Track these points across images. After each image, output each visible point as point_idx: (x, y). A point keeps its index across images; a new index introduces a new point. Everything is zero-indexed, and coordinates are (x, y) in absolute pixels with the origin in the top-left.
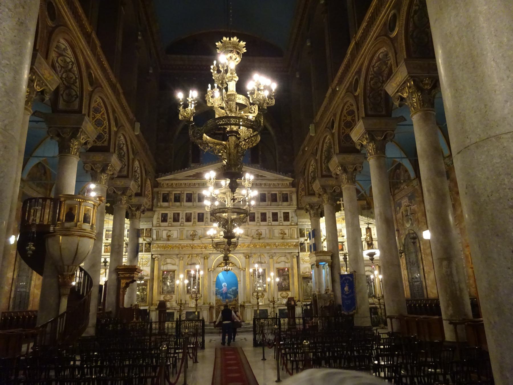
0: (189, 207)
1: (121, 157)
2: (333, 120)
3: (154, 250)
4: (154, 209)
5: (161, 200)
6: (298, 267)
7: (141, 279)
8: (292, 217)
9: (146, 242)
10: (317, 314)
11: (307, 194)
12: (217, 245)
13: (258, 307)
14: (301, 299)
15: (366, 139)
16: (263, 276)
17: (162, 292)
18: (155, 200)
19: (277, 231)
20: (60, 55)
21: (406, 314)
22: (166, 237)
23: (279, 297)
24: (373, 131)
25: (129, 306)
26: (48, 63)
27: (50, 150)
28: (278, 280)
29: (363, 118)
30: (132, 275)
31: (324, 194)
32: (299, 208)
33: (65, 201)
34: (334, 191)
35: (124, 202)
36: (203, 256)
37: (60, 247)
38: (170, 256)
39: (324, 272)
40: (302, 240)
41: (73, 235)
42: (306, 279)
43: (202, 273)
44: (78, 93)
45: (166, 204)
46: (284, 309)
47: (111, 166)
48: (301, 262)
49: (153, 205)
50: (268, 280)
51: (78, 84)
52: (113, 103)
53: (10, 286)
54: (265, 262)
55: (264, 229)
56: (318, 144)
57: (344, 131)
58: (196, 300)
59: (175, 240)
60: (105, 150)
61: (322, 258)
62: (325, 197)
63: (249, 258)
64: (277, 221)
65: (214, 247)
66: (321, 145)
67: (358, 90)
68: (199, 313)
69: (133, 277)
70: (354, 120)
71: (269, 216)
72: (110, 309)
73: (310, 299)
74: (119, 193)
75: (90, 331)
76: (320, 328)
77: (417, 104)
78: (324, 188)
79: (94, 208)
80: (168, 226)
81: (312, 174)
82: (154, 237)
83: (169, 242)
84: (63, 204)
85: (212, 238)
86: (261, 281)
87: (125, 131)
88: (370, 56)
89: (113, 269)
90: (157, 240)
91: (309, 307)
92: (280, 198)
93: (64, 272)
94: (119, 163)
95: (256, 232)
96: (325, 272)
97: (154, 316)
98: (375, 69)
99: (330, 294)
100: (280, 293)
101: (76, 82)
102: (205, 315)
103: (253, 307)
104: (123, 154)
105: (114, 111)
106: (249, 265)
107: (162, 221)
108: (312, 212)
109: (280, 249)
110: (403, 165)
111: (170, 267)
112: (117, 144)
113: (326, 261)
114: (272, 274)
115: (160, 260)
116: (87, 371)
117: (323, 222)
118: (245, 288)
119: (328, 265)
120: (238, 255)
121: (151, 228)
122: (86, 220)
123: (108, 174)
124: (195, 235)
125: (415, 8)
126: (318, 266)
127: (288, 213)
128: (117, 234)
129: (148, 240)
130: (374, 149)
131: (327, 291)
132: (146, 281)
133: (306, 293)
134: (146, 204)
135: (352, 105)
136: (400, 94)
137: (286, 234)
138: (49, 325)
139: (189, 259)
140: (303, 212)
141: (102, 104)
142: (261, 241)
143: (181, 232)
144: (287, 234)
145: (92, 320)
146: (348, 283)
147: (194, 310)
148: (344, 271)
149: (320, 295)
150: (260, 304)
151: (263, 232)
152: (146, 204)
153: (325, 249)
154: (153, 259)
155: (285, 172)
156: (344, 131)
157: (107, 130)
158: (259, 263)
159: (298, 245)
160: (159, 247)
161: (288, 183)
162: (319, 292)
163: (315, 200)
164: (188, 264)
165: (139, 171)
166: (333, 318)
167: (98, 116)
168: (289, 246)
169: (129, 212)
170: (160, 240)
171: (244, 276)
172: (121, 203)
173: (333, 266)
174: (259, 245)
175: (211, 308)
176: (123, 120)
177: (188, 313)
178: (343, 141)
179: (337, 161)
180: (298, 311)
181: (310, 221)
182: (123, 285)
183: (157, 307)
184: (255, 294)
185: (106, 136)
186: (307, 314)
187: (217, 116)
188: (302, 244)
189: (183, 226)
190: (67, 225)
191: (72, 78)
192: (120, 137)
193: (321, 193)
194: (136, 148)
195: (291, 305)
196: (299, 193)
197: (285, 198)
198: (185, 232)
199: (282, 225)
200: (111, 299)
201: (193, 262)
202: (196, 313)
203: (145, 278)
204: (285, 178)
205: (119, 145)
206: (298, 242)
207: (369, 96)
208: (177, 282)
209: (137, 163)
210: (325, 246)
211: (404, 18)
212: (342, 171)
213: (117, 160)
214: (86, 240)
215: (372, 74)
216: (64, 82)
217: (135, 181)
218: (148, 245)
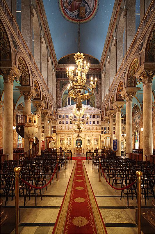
0: (67, 119)
20: (21, 64)
26: (16, 67)
27: (22, 100)
32: (102, 120)
35: (47, 117)
42: (103, 142)
48: (101, 137)
59: (63, 129)
70: (122, 89)
74: (45, 114)
75: (40, 154)
76: (106, 156)
88: (132, 61)
94: (44, 104)
97: (58, 151)
98: (132, 68)
102: (72, 151)
105: (31, 68)
116: (148, 182)
125: (151, 39)
145: (40, 151)
163: (107, 117)
167: (36, 87)
171: (84, 141)
180: (100, 151)
182: (48, 142)
186: (102, 152)
187: (106, 227)
190: (29, 123)
191: (26, 73)
195: (97, 150)
198: (66, 127)
211: (146, 44)
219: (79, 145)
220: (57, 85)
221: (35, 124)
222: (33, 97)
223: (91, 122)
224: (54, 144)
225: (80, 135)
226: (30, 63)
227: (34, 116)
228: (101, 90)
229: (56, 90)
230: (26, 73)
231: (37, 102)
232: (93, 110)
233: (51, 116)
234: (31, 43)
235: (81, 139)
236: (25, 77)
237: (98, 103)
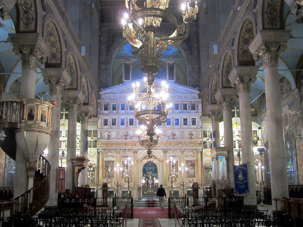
0: (123, 114)
1: (71, 74)
2: (233, 38)
3: (99, 146)
4: (98, 116)
5: (103, 109)
7: (90, 167)
8: (198, 122)
9: (93, 140)
10: (215, 195)
11: (210, 103)
12: (142, 143)
13: (172, 189)
14: (203, 184)
15: (263, 50)
16: (176, 166)
17: (105, 177)
18: (99, 109)
19: (186, 133)
21: (288, 197)
22: (107, 136)
23: (188, 182)
24: (269, 43)
25: (82, 186)
28: (187, 169)
29: (236, 67)
30: (82, 164)
31: (223, 102)
32: (203, 115)
33: (27, 104)
34: (232, 100)
36: (133, 151)
37: (25, 140)
38: (110, 151)
39: (221, 163)
40: (205, 139)
41: (34, 131)
42: (208, 169)
43: (132, 163)
44: (34, 17)
45: (106, 112)
46: (191, 191)
47: (63, 79)
48: (204, 156)
49: (97, 113)
50: (180, 169)
51: (33, 9)
52: (63, 28)
53: (4, 169)
56: (220, 60)
57: (242, 47)
58: (128, 183)
60: (58, 66)
61: (220, 152)
62: (224, 104)
63: (166, 153)
64: (187, 125)
65: (141, 144)
66: (222, 61)
67: (257, 7)
68: (130, 192)
69: (83, 165)
71: (181, 121)
72: (68, 188)
73: (210, 184)
77: (267, 61)
78: (224, 97)
79: (48, 110)
80: (108, 129)
81: (214, 87)
82: (99, 136)
83: (109, 141)
84: (25, 107)
85: (139, 137)
86: (174, 170)
87: (74, 52)
89: (69, 159)
90: (101, 138)
91: (208, 190)
92: (189, 107)
93: (30, 159)
95: (172, 134)
96: (222, 163)
97: (100, 194)
99: (226, 181)
100: (188, 179)
101: (32, 7)
102: (135, 195)
103: (168, 189)
104: (73, 71)
105: (64, 35)
106: (165, 158)
107: (104, 125)
108: (213, 117)
109: (189, 146)
110: (286, 78)
111: (111, 159)
112: (67, 63)
113: (224, 155)
114: (183, 164)
115: (103, 153)
117: (222, 126)
118: (163, 174)
119: (225, 158)
120: (158, 151)
121: (96, 130)
122: (43, 119)
123: (61, 86)
124: (128, 135)
126: (217, 159)
128: (71, 135)
129: (95, 138)
130: (268, 59)
131: (223, 177)
132: (94, 169)
133: (207, 179)
134: (92, 111)
135: (251, 23)
136: (298, 2)
137: (193, 135)
138: (20, 198)
139: (123, 153)
140: (207, 118)
141: (54, 28)
142: (174, 140)
143: (118, 133)
144: (194, 135)
146: (242, 172)
147: (127, 190)
148: (237, 164)
149: (218, 180)
150: (174, 186)
152: (92, 111)
153: (222, 146)
154: (98, 153)
155: (194, 86)
157: (59, 50)
158: (173, 156)
160: (102, 144)
162: (218, 178)
163: (216, 107)
164: (123, 157)
165: (86, 86)
166: (228, 199)
167: (52, 39)
168: (195, 144)
169: (80, 117)
170: (103, 139)
171: (163, 166)
172: (73, 110)
173: (229, 159)
174: (174, 143)
175: (139, 189)
176: (72, 43)
177: (123, 192)
178: (241, 56)
179: (236, 73)
180: (201, 192)
181: (211, 124)
183: (101, 187)
184: (170, 179)
185: (59, 55)
186: (209, 195)
188: (205, 142)
189: (119, 129)
190: (29, 122)
191: (28, 4)
192: (70, 58)
193: (221, 102)
194: (82, 67)
195: (196, 188)
196: (204, 103)
197: (193, 108)
198: (120, 133)
199: (191, 128)
200: (68, 180)
201: (126, 155)
202: (129, 192)
203: (94, 166)
204: (194, 91)
205: (70, 64)
206: (202, 141)
207: (267, 11)
208: (115, 169)
209: (84, 80)
210: (222, 144)
212: (240, 81)
213: (69, 76)
214: (43, 134)
215: (226, 64)
216: (23, 7)
217: (83, 94)
218: (95, 143)
219: (150, 177)
220: (102, 38)
221: (43, 124)
222: (42, 58)
223: (178, 120)
224: (92, 174)
225: (154, 152)
226: (65, 30)
227: (41, 104)
229: (100, 48)
230: (28, 4)
231: (52, 72)
232: (181, 91)
233: (85, 107)
235: (155, 161)
236: (26, 12)
237: (194, 75)
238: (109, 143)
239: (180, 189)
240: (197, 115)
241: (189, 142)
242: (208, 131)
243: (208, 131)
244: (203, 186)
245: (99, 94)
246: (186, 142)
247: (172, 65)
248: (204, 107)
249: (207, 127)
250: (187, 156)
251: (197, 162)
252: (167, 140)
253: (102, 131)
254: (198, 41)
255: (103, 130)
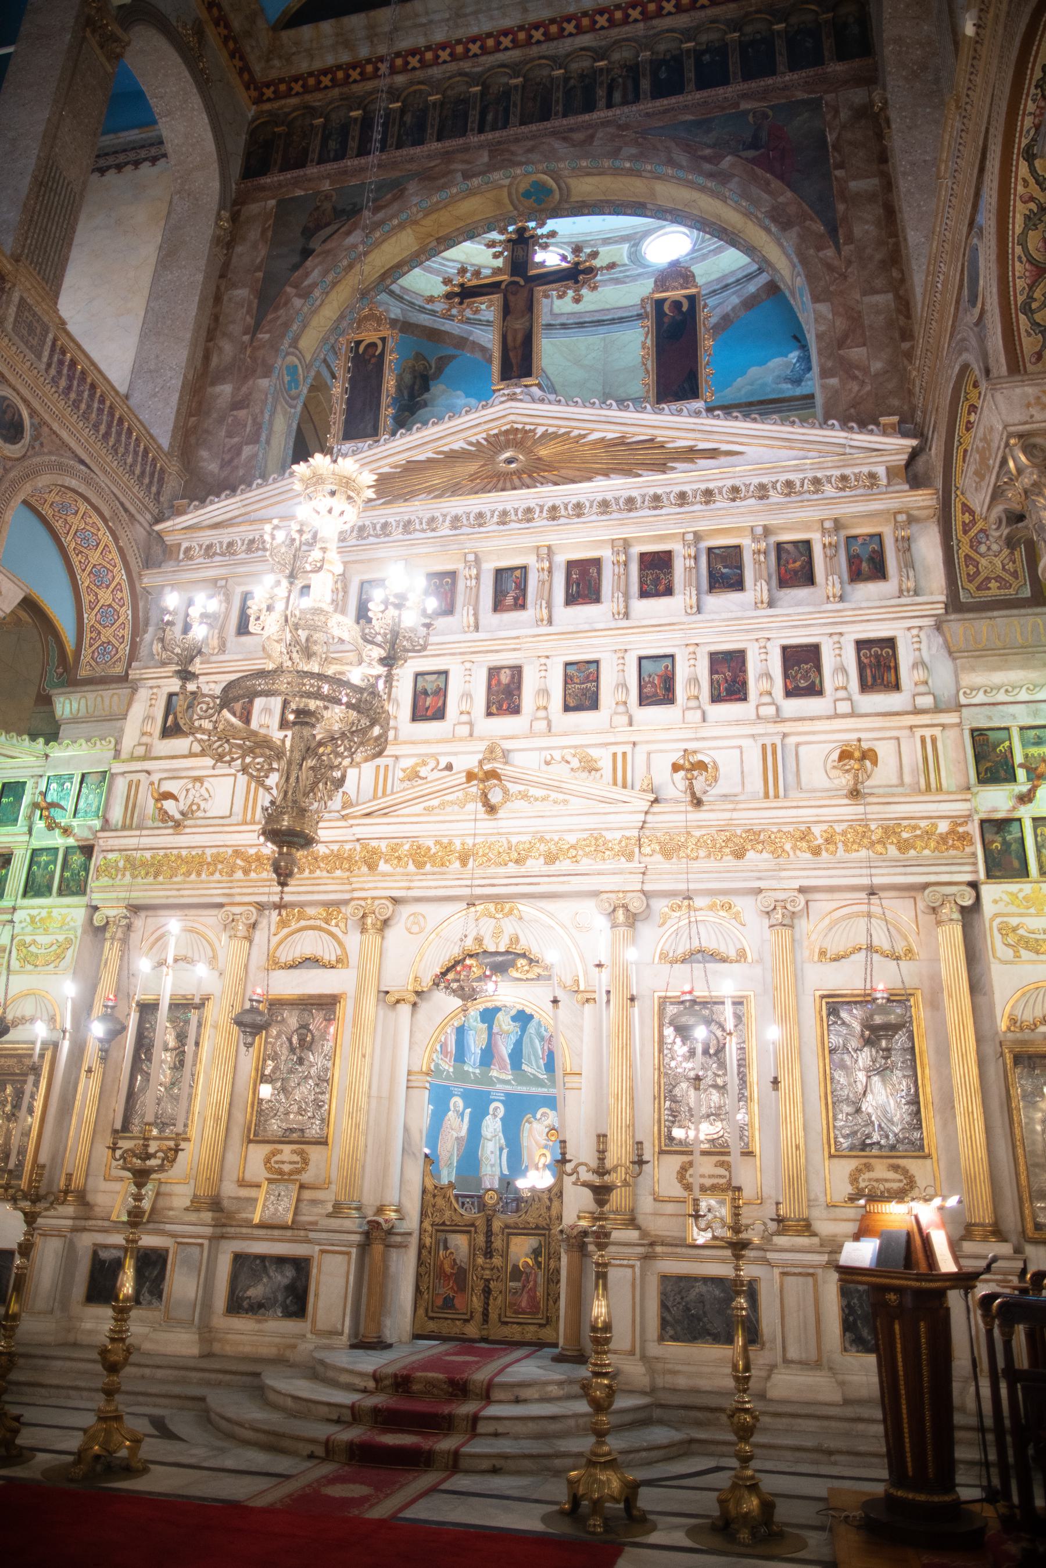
4: (133, 674)
6: (977, 985)
9: (71, 841)
32: (954, 605)
48: (996, 947)
54: (742, 955)
55: (730, 737)
64: (820, 693)
92: (830, 558)
127: (890, 643)
151: (726, 760)
156: (993, 584)
159: (965, 838)
161: (881, 471)
168: (904, 846)
170: (140, 827)
197: (867, 563)
199: (853, 714)
218: (77, 859)
228: (888, 185)
234: (42, 1056)
238: (179, 857)
239: (768, 1263)
240: (898, 612)
241: (839, 828)
242: (1015, 734)
243: (1022, 728)
244: (1018, 1250)
245: (159, 535)
246: (817, 830)
247: (685, 309)
248: (965, 549)
249: (1001, 697)
250: (832, 951)
251: (935, 1004)
252: (642, 817)
253: (143, 776)
254: (883, 157)
255: (148, 765)
